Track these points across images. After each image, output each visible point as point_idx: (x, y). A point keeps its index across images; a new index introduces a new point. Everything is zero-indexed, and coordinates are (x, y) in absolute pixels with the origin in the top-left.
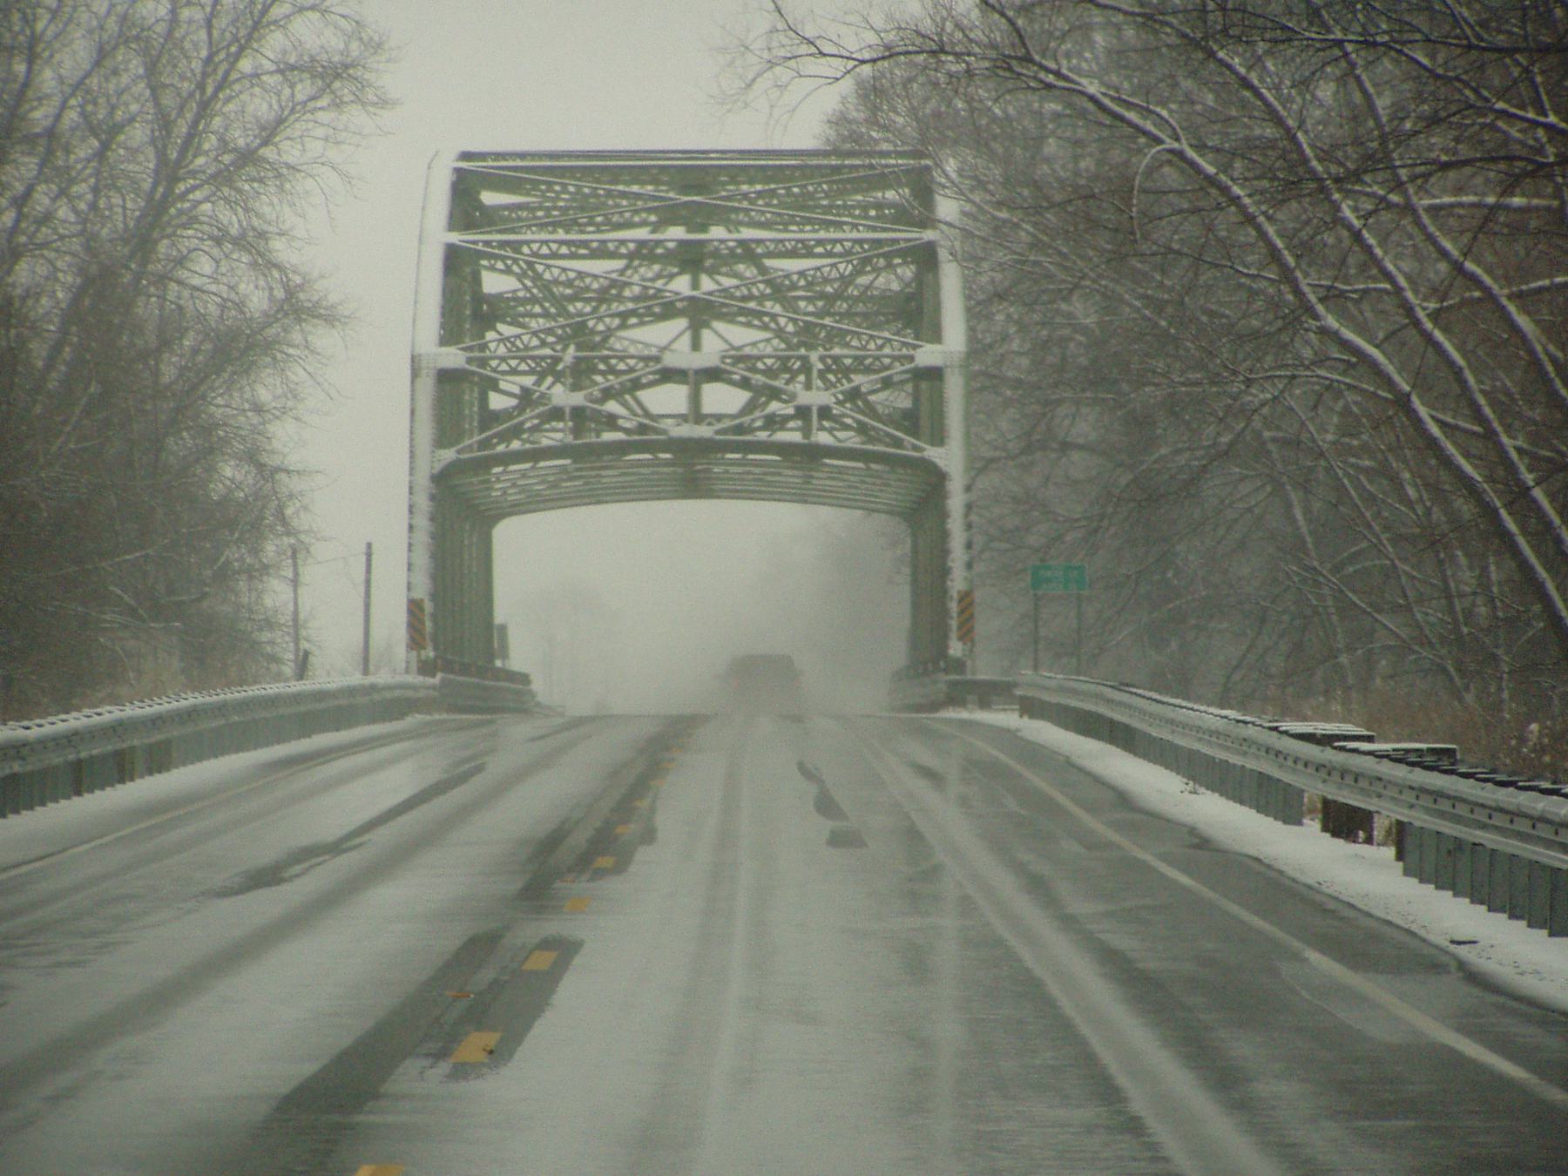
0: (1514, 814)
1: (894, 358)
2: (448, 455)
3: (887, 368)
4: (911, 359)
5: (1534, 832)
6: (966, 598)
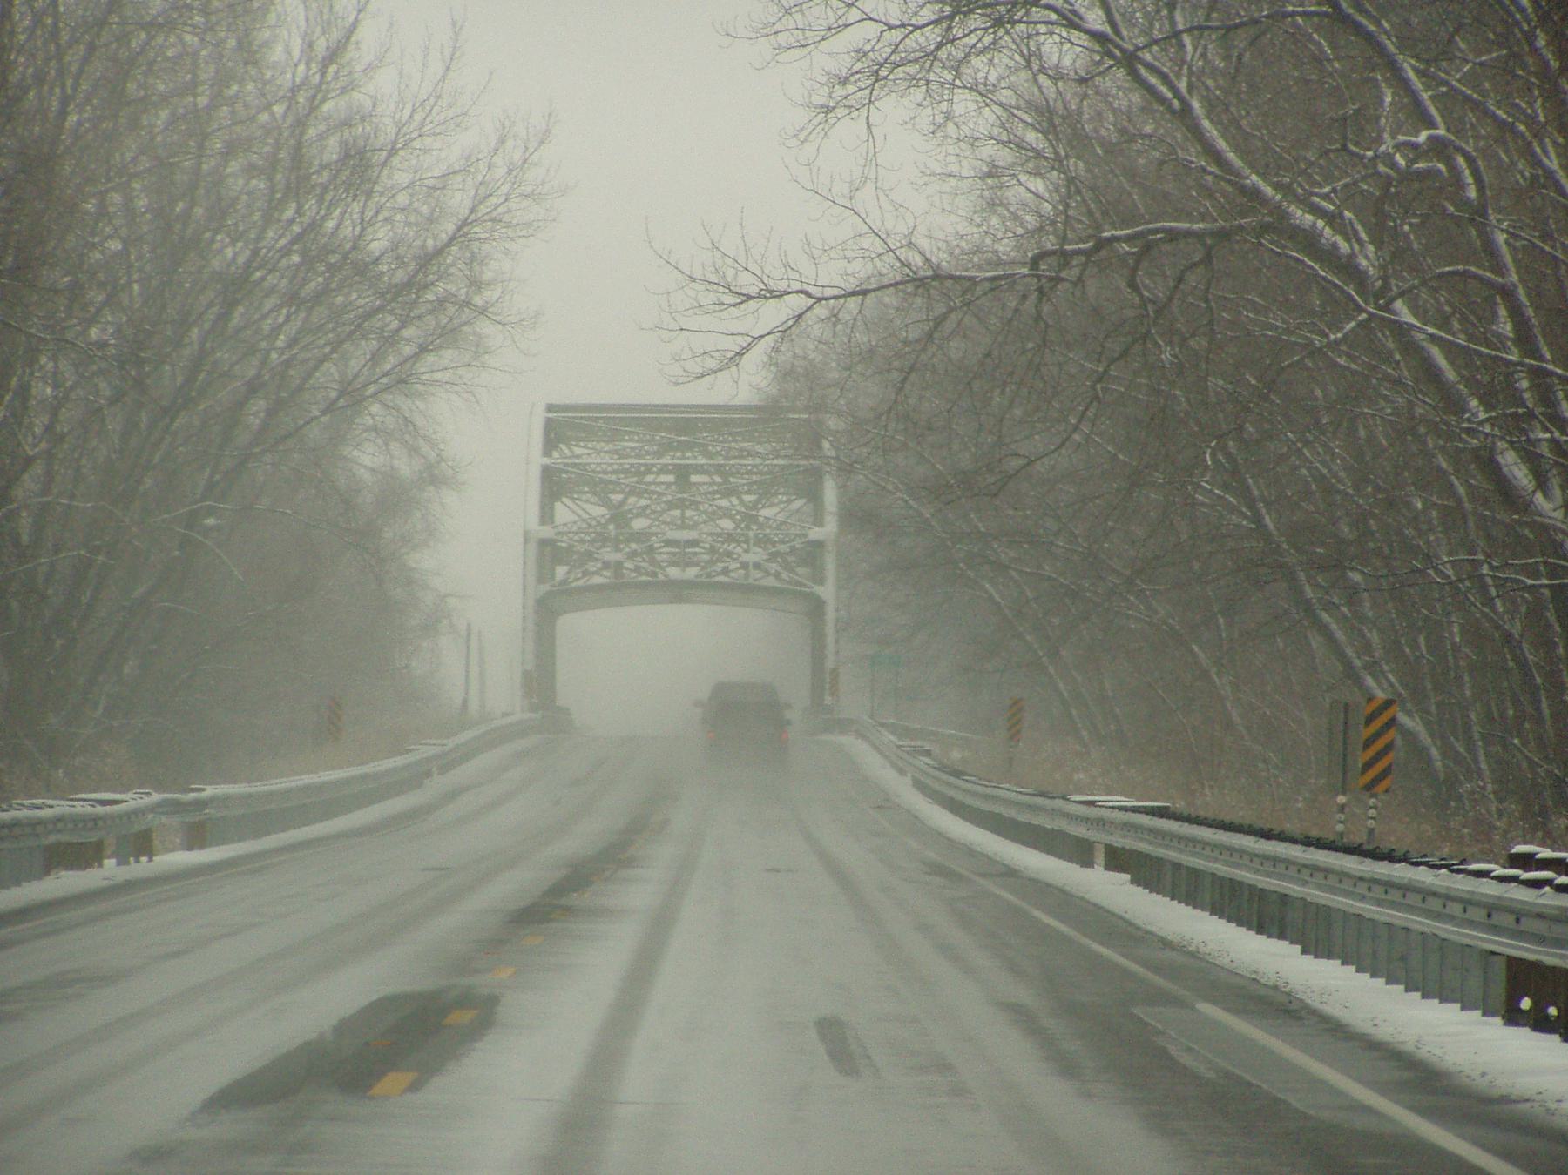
0: (1389, 885)
1: (796, 535)
2: (545, 588)
3: (793, 541)
4: (805, 536)
5: (1423, 906)
6: (835, 673)
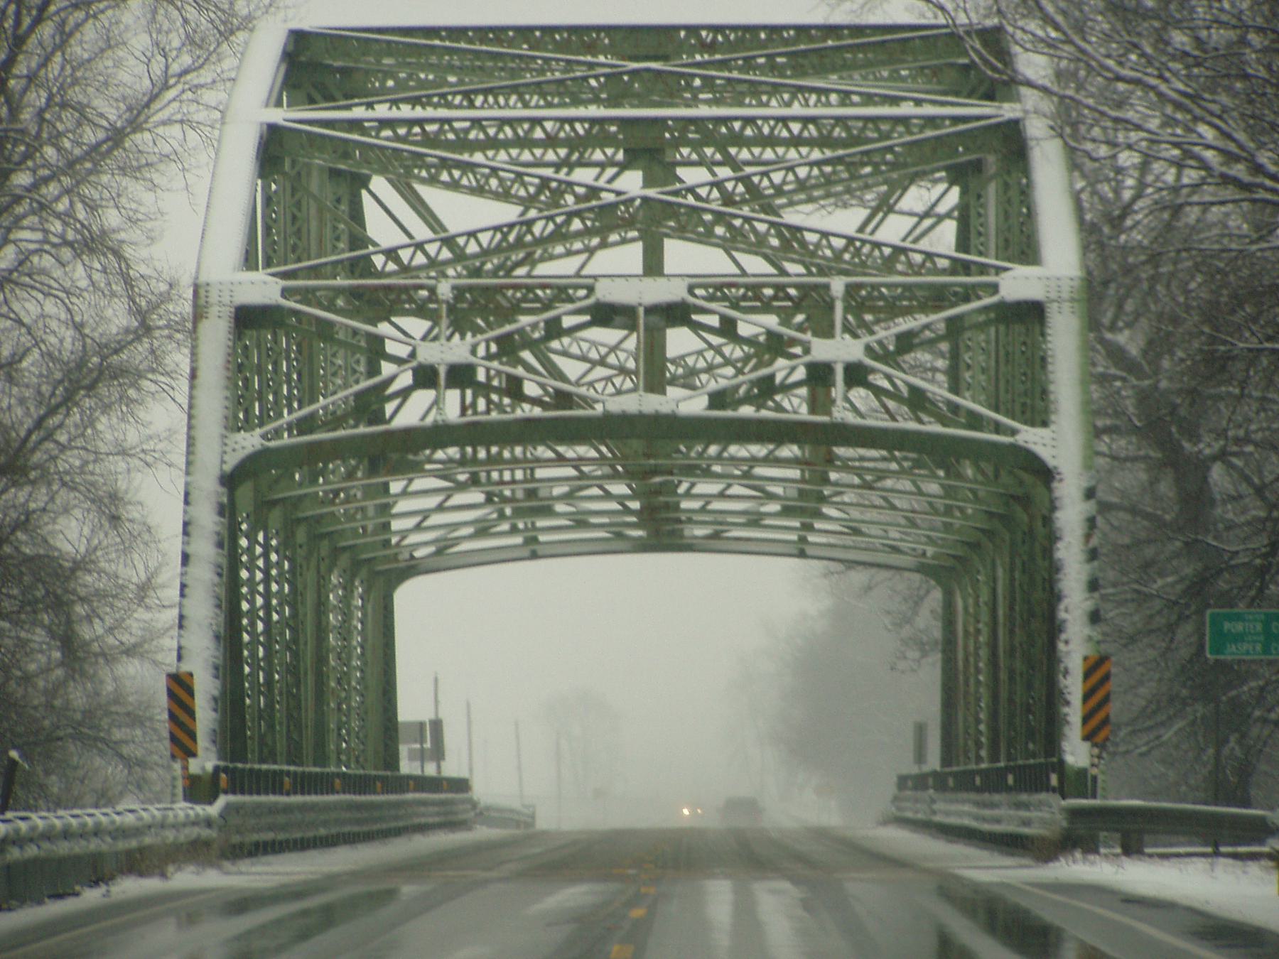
2: (250, 441)
